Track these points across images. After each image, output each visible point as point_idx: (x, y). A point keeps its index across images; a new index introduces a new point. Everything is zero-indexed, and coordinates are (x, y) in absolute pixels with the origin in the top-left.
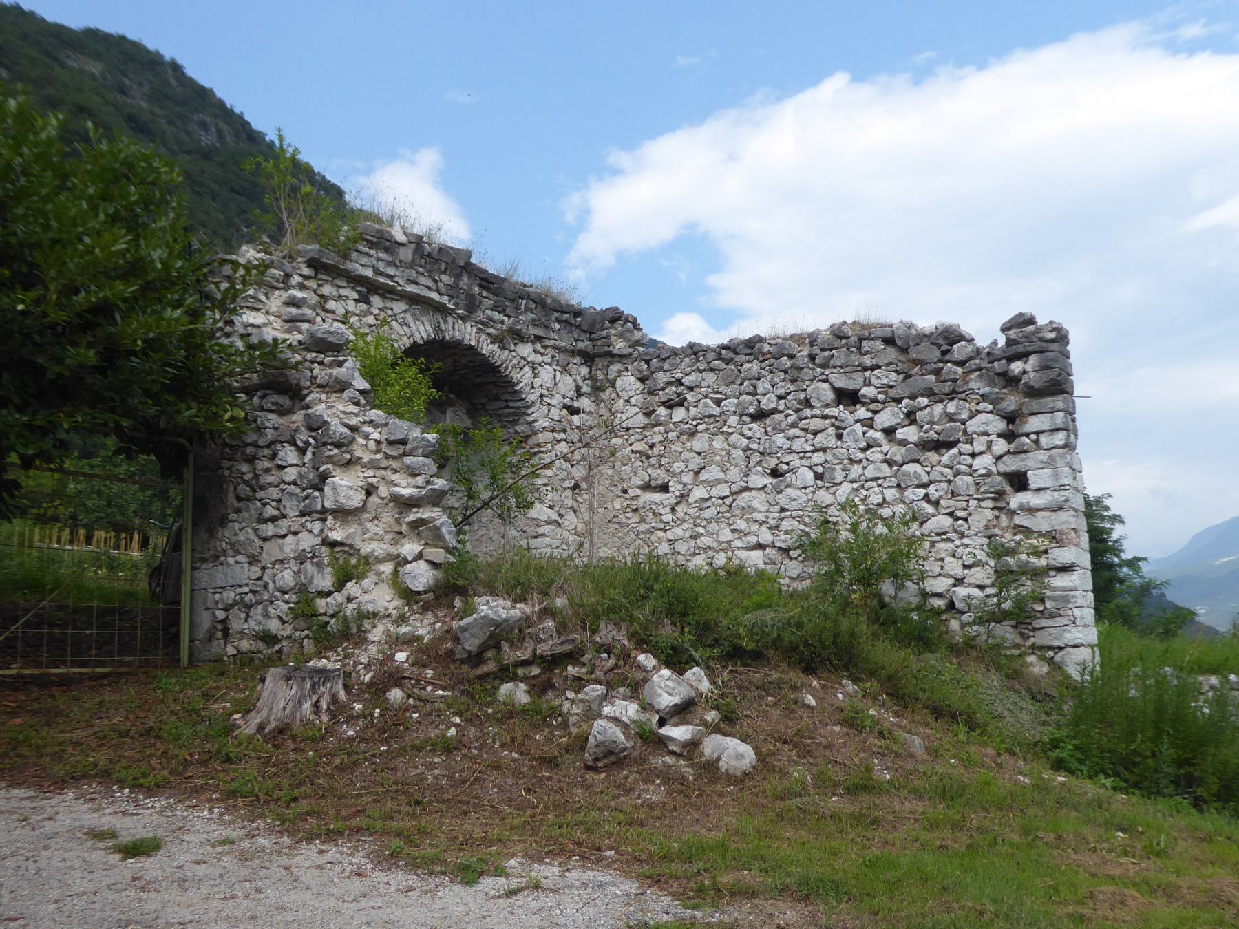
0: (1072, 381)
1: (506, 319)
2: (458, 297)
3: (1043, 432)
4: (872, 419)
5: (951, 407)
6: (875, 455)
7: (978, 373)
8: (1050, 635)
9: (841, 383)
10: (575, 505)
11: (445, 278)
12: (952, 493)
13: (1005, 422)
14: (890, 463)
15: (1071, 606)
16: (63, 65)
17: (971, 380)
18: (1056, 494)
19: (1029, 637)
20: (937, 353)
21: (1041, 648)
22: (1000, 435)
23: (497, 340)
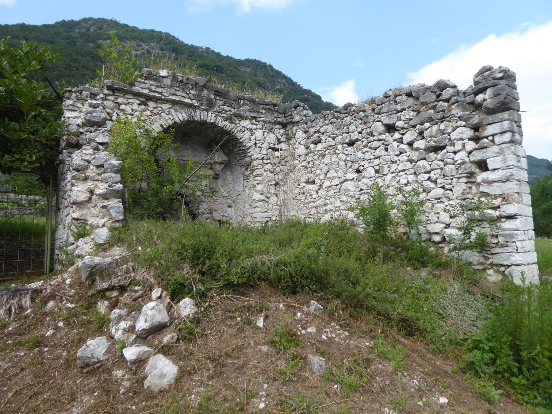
0: (519, 103)
1: (233, 109)
2: (202, 100)
3: (496, 134)
4: (402, 138)
5: (442, 126)
6: (403, 157)
7: (456, 104)
8: (502, 257)
9: (387, 121)
10: (277, 192)
11: (193, 92)
12: (444, 175)
13: (473, 131)
14: (411, 161)
15: (514, 240)
16: (239, 71)
17: (452, 109)
18: (504, 171)
19: (489, 259)
20: (434, 97)
21: (496, 265)
22: (470, 139)
23: (229, 119)
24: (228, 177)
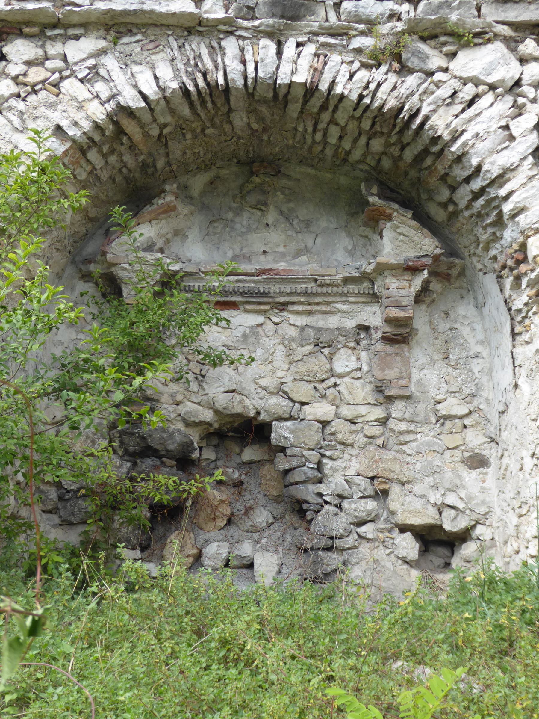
24: (466, 331)
